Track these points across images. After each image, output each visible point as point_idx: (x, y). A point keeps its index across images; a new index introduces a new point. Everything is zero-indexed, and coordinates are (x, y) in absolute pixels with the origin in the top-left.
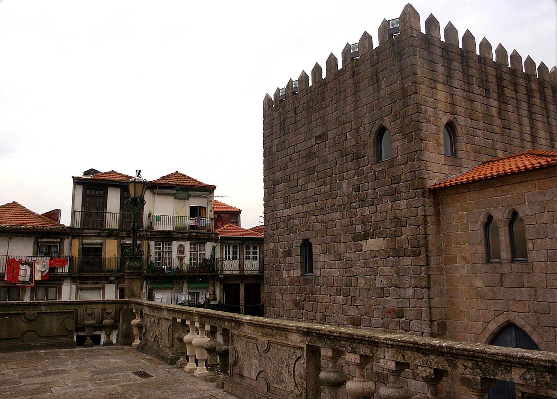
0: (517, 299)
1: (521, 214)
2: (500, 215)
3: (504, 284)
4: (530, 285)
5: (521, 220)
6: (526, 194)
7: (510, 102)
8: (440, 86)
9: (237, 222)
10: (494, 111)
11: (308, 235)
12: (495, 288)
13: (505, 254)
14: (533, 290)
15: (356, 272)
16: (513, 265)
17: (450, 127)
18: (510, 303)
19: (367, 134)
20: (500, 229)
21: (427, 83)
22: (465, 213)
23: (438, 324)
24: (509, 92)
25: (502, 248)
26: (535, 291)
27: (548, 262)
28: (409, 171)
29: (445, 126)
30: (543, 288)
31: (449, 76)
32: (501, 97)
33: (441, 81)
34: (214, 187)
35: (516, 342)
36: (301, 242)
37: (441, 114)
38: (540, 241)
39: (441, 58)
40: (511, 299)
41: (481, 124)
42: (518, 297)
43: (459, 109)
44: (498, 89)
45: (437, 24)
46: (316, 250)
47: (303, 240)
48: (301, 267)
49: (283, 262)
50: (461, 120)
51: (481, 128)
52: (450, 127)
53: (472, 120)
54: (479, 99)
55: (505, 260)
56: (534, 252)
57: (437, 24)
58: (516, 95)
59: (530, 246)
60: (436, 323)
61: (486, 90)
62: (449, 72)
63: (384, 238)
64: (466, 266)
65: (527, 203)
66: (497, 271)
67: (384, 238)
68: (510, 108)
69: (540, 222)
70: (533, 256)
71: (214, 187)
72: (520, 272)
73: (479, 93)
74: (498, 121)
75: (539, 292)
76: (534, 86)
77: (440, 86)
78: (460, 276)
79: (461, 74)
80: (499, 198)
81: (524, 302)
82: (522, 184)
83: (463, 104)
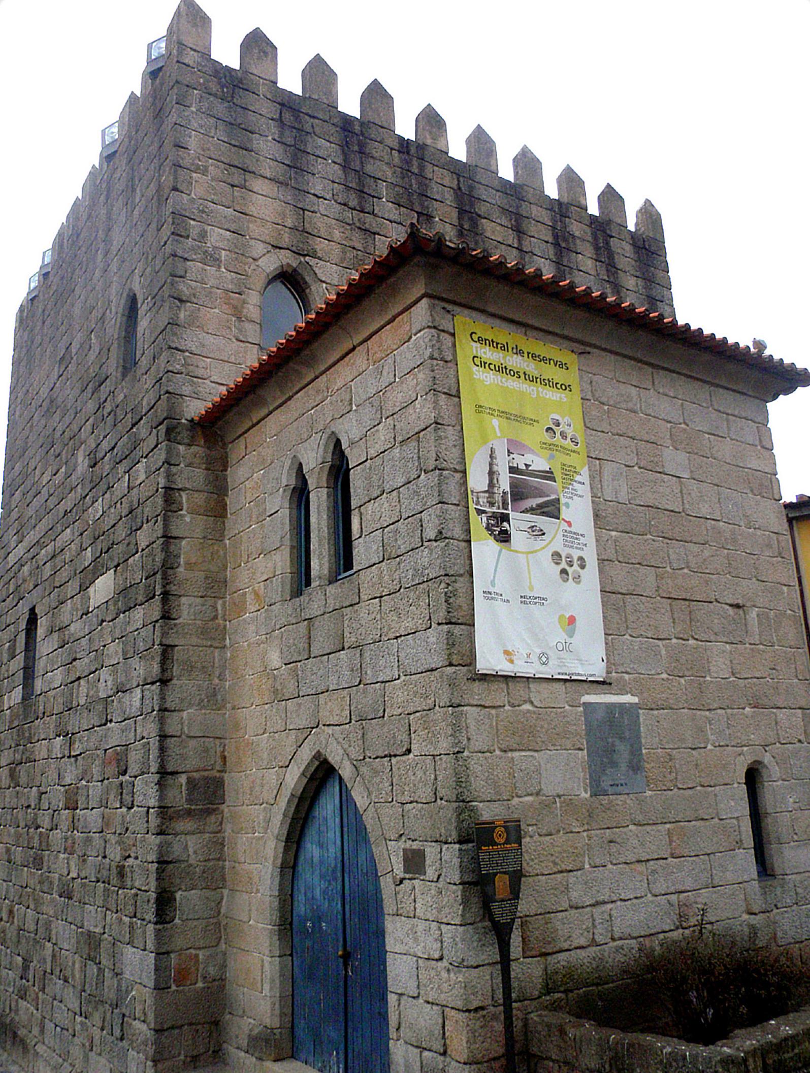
2: (314, 458)
23: (190, 781)
37: (259, 248)
43: (320, 246)
57: (269, 49)
58: (519, 240)
60: (183, 779)
77: (258, 185)
83: (337, 235)
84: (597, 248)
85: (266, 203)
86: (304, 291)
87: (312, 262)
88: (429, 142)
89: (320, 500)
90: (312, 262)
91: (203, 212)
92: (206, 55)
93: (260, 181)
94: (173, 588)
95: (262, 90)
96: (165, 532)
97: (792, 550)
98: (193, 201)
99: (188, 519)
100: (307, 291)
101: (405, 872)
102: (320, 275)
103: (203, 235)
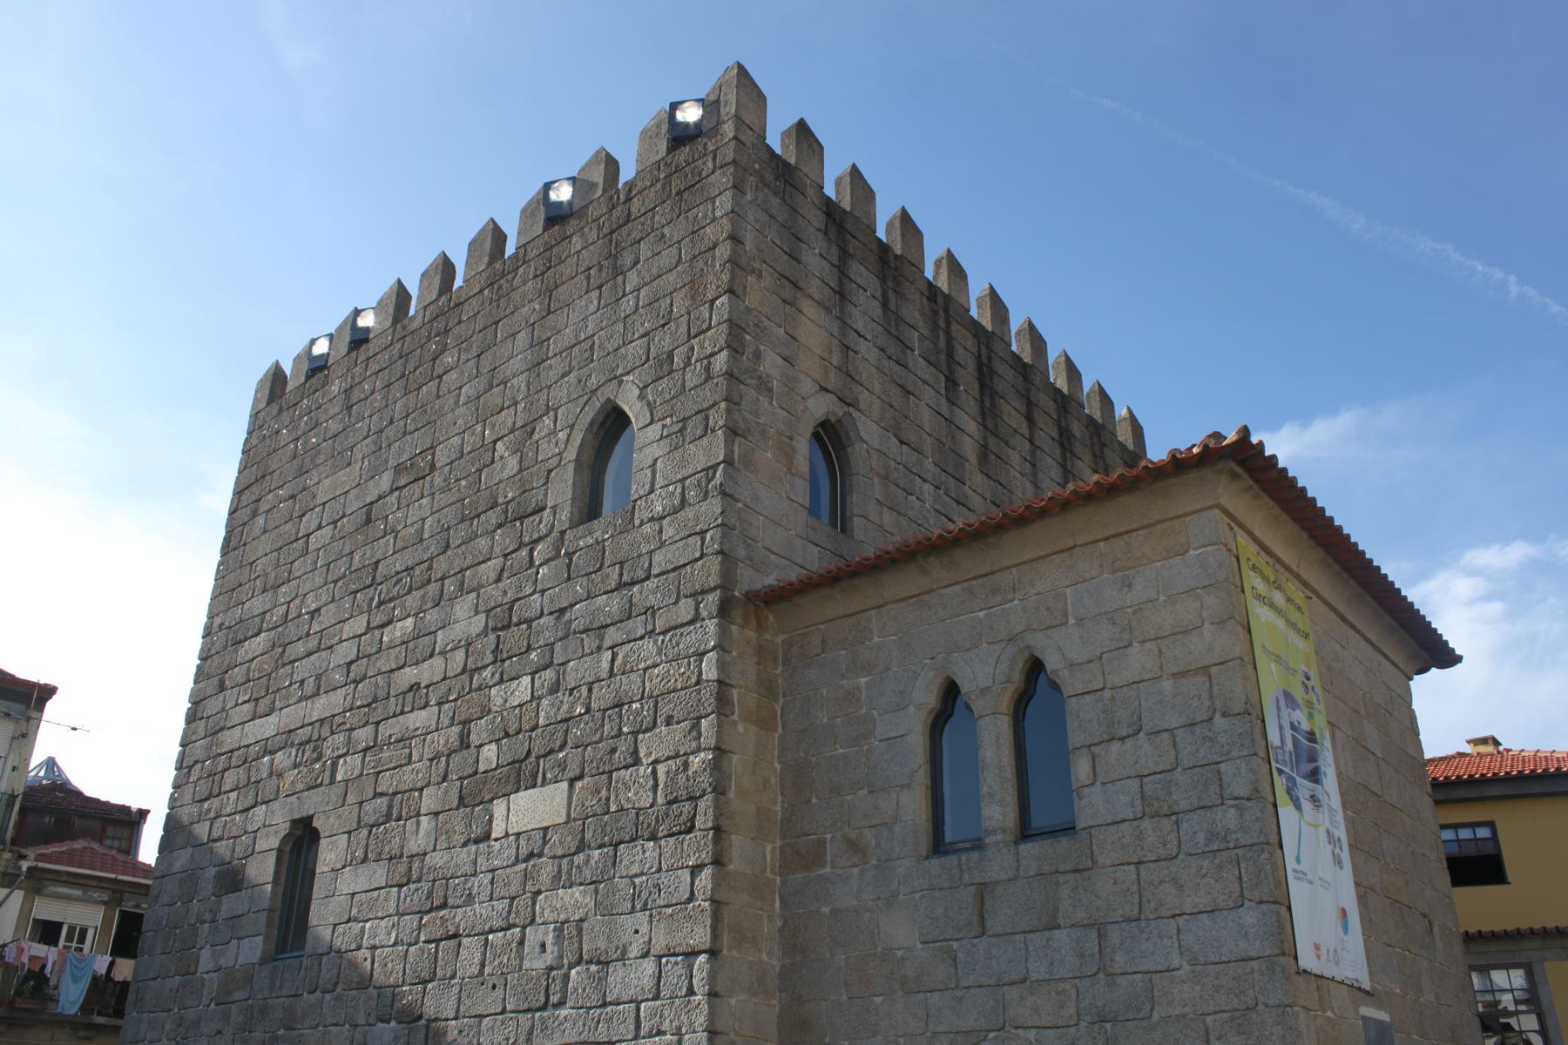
0: (1034, 976)
1: (1052, 663)
2: (987, 677)
3: (988, 924)
4: (1081, 915)
5: (1055, 686)
6: (1069, 590)
7: (1012, 442)
8: (809, 308)
9: (25, 738)
10: (969, 448)
11: (310, 804)
12: (955, 945)
13: (999, 812)
14: (1094, 934)
15: (460, 918)
16: (1026, 848)
17: (831, 439)
18: (1012, 993)
19: (562, 442)
20: (982, 723)
21: (768, 279)
22: (863, 680)
24: (1011, 414)
25: (985, 790)
26: (1100, 937)
27: (1146, 823)
28: (682, 534)
29: (816, 435)
30: (1129, 920)
31: (841, 294)
32: (988, 415)
33: (816, 296)
34: (47, 692)
35: (1188, 515)
36: (284, 828)
38: (1115, 746)
39: (820, 235)
40: (1014, 977)
41: (929, 466)
42: (1037, 969)
43: (863, 396)
44: (982, 393)
45: (816, 147)
46: (329, 855)
47: (294, 822)
48: (269, 924)
49: (208, 916)
50: (869, 432)
51: (927, 476)
52: (831, 439)
53: (902, 442)
54: (928, 395)
55: (994, 832)
56: (1098, 788)
57: (816, 147)
59: (1081, 768)
61: (947, 379)
62: (840, 283)
63: (349, 833)
64: (856, 870)
65: (1072, 621)
66: (966, 877)
67: (572, 781)
68: (1015, 458)
69: (1116, 681)
70: (1092, 807)
71: (46, 692)
72: (1046, 869)
73: (923, 376)
74: (979, 479)
75: (1114, 936)
76: (1077, 429)
77: (809, 308)
78: (835, 913)
79: (876, 304)
80: (981, 614)
81: (1061, 986)
82: (1057, 559)
83: (877, 388)
84: (1095, 456)
85: (814, 328)
86: (844, 448)
87: (856, 414)
88: (954, 294)
89: (993, 739)
90: (856, 414)
91: (756, 325)
92: (762, 137)
93: (809, 302)
94: (725, 823)
95: (811, 193)
96: (718, 741)
97: (947, 790)
98: (748, 310)
99: (741, 728)
100: (849, 450)
101: (56, 945)
102: (862, 433)
103: (757, 356)
